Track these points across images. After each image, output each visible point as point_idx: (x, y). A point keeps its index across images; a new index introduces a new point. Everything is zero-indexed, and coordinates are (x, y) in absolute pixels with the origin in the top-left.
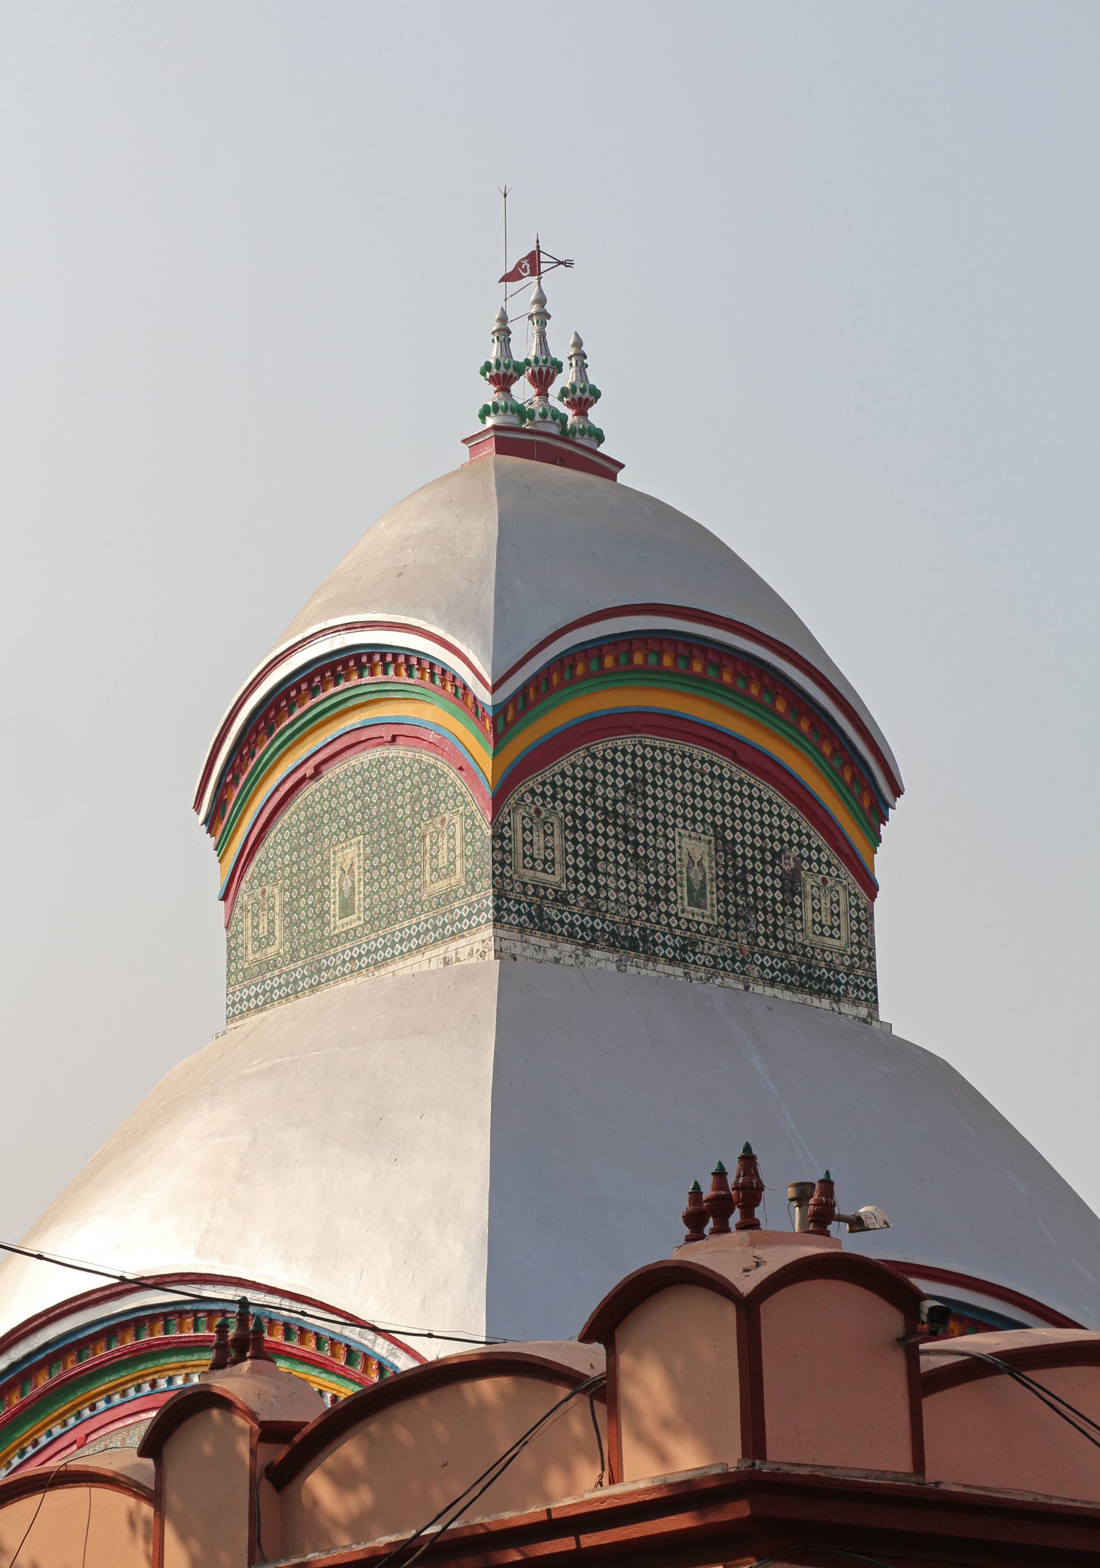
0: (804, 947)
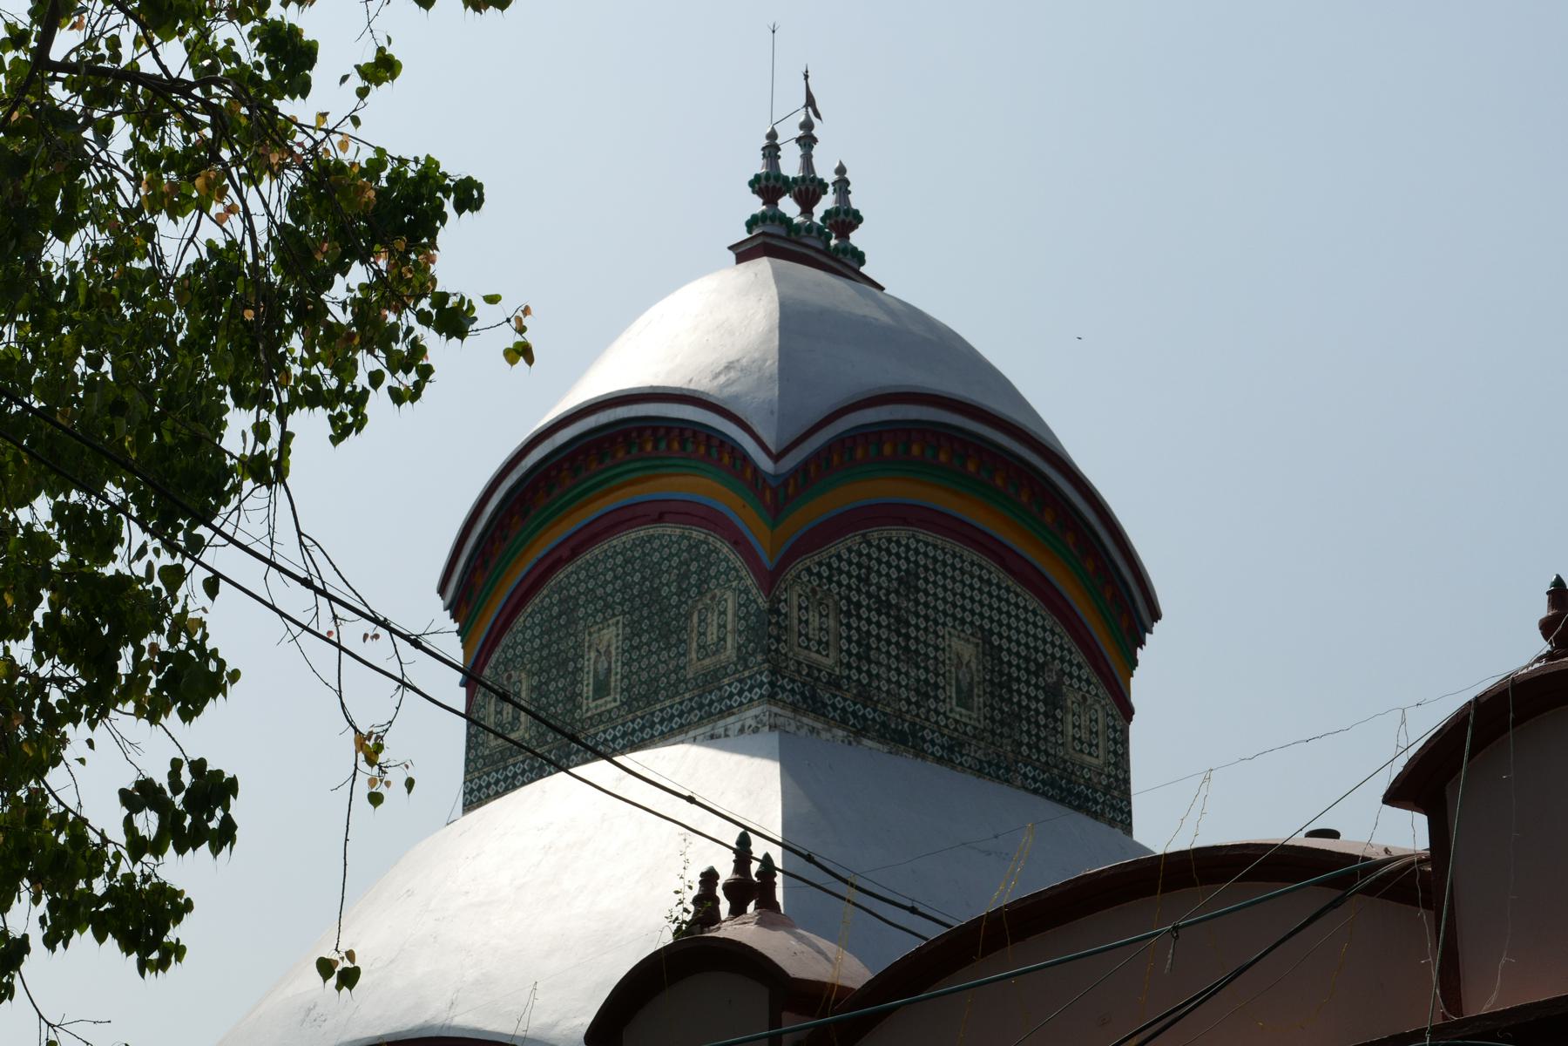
0: (1065, 762)
